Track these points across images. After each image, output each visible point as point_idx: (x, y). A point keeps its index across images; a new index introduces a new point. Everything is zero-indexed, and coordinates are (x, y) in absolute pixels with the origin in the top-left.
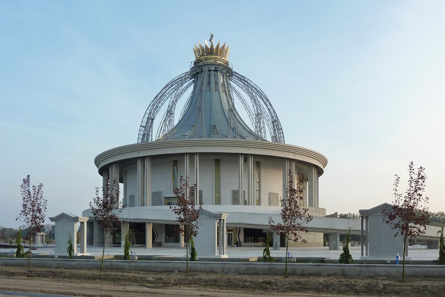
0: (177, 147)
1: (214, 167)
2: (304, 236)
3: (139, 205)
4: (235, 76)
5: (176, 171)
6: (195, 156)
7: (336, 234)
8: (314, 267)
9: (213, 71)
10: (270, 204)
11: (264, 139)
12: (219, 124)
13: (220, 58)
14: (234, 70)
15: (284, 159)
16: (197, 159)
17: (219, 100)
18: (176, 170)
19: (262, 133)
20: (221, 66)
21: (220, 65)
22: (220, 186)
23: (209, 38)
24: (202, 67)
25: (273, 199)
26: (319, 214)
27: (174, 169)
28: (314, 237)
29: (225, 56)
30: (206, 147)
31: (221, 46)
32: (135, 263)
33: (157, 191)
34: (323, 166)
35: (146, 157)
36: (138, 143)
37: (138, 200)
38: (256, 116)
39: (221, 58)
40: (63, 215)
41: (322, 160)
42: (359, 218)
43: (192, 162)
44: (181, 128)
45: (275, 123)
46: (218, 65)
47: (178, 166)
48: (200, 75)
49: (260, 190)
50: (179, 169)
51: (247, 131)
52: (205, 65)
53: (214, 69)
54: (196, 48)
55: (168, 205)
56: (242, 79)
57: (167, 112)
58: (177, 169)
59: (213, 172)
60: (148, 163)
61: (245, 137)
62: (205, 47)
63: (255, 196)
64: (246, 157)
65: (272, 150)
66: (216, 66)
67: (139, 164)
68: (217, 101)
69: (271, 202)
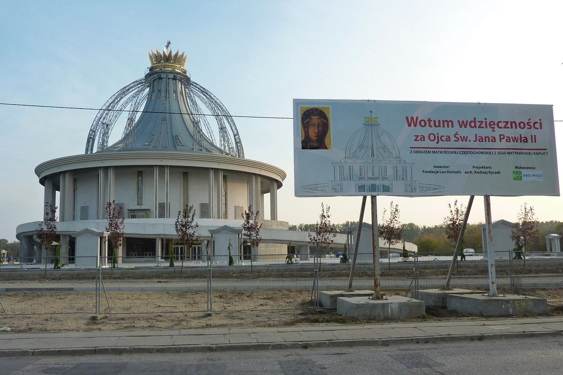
1: (182, 180)
2: (271, 249)
4: (193, 85)
5: (140, 182)
6: (165, 169)
7: (306, 246)
8: (331, 266)
9: (172, 79)
10: (236, 218)
11: (228, 152)
12: (181, 134)
13: (179, 66)
14: (192, 79)
15: (250, 174)
16: (167, 171)
17: (178, 109)
18: (141, 181)
20: (180, 75)
21: (179, 74)
22: (188, 199)
23: (166, 44)
24: (160, 74)
25: (239, 213)
26: (284, 227)
27: (138, 179)
28: (280, 250)
29: (183, 65)
31: (179, 54)
32: (196, 268)
33: (117, 203)
35: (66, 171)
38: (220, 129)
39: (180, 67)
40: (86, 230)
41: (280, 174)
42: (298, 231)
43: (162, 174)
44: (139, 136)
46: (177, 74)
47: (143, 176)
48: (158, 82)
49: (226, 204)
50: (144, 180)
51: (209, 142)
52: (163, 72)
53: (172, 77)
54: (152, 53)
55: (132, 218)
56: (204, 91)
58: (142, 180)
60: (111, 174)
61: (211, 151)
62: (162, 54)
63: (223, 209)
64: (216, 170)
65: (240, 166)
66: (175, 75)
67: (101, 173)
69: (236, 215)
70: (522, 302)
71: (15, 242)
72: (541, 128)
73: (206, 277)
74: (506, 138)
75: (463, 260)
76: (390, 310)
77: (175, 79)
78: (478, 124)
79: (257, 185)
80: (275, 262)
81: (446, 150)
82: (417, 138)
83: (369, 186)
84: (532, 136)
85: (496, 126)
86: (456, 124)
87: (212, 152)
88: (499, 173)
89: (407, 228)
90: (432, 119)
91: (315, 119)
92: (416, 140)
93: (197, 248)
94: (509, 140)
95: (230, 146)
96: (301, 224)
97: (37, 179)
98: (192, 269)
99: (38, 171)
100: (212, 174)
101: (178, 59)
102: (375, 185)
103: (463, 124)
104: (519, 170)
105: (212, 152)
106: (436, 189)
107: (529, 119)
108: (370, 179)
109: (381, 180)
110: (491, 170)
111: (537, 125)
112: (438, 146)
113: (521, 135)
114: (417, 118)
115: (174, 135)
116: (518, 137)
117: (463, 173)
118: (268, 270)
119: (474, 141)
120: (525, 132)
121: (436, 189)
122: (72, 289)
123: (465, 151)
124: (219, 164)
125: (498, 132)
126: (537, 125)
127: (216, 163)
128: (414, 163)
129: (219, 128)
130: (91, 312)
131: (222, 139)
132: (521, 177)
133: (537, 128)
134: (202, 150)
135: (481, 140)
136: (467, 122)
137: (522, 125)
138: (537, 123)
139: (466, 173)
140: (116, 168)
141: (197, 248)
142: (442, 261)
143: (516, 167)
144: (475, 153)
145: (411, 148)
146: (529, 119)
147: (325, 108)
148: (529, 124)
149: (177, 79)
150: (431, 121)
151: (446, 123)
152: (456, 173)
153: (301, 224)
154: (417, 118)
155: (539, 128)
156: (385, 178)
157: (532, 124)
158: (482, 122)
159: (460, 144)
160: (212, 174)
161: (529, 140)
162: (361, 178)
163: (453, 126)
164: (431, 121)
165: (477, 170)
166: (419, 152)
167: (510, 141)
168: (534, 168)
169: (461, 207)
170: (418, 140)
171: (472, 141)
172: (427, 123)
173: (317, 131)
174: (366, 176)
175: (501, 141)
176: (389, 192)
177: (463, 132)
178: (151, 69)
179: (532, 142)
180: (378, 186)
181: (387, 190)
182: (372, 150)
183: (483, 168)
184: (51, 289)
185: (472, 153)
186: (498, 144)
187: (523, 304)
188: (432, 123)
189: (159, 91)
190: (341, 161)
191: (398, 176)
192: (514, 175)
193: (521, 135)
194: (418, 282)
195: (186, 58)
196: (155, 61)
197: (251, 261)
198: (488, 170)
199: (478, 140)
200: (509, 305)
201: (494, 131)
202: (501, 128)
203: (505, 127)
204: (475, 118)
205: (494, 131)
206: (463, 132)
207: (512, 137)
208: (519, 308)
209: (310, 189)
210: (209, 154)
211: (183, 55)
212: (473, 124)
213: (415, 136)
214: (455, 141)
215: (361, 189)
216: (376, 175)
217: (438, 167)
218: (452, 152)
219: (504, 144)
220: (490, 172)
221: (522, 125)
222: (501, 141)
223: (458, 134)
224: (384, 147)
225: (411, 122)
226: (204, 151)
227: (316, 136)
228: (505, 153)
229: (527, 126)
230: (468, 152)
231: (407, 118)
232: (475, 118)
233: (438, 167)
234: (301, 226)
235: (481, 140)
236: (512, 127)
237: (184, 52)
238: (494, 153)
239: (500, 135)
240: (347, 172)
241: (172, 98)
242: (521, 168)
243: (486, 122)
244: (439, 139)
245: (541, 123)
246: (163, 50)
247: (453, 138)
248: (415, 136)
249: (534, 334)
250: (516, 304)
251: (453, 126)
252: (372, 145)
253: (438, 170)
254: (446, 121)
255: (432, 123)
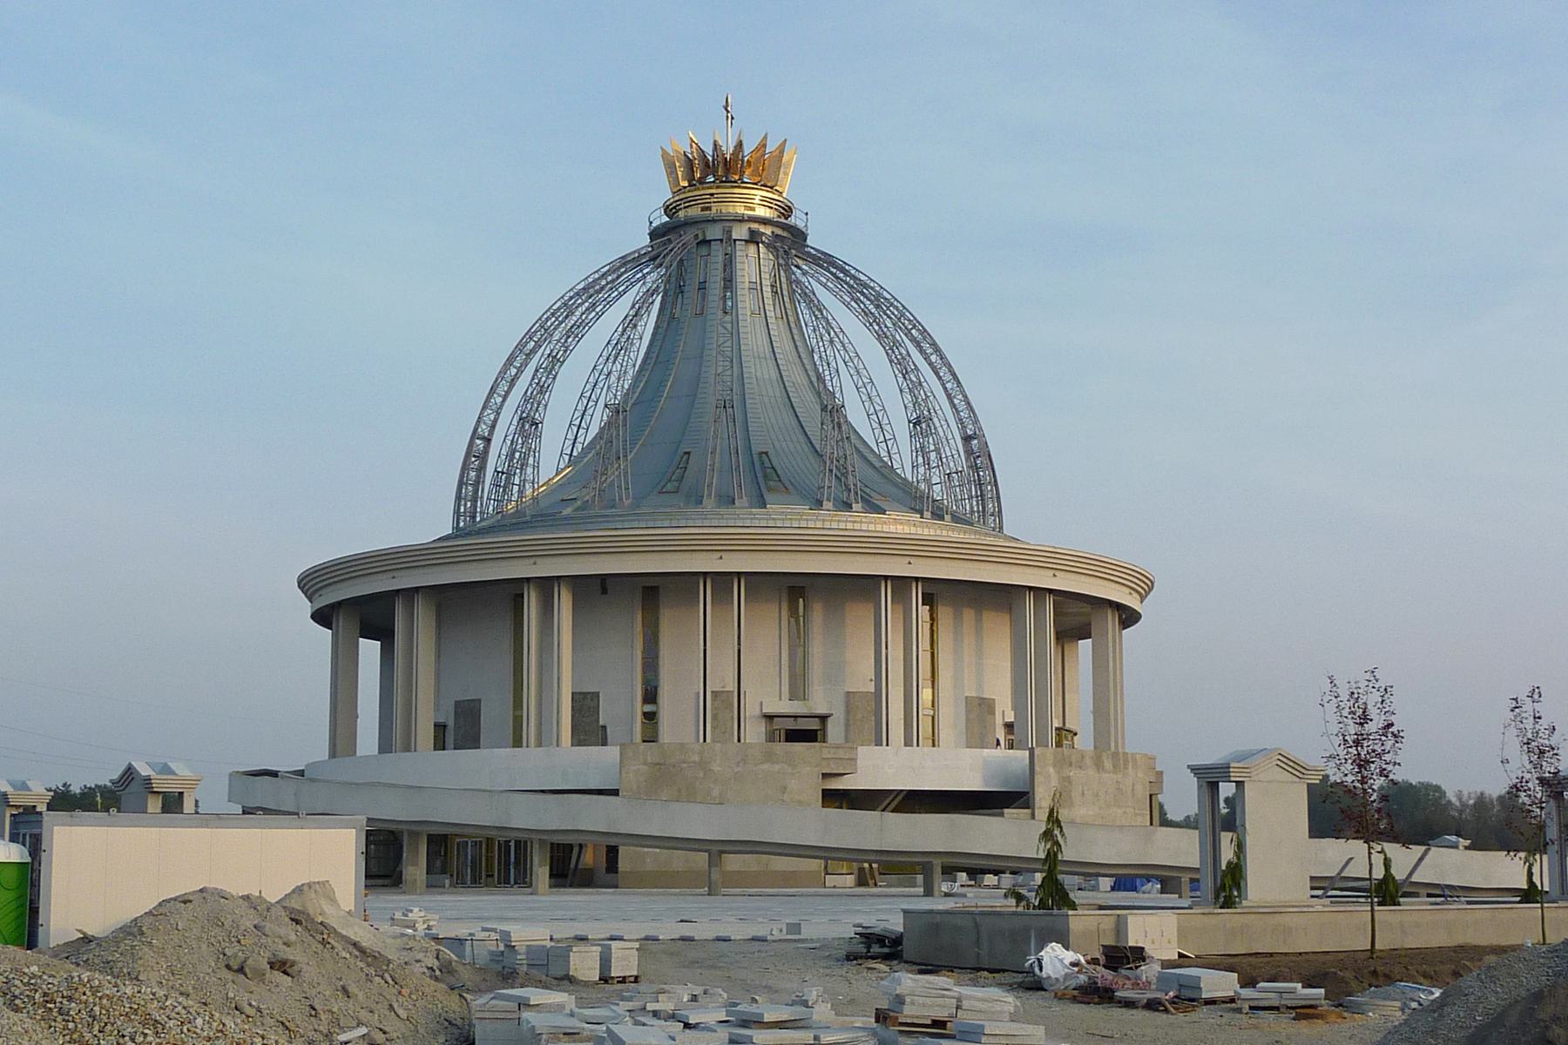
0: (370, 574)
3: (398, 749)
19: (917, 465)
30: (561, 559)
34: (1141, 597)
35: (417, 589)
36: (468, 529)
37: (494, 714)
38: (911, 425)
45: (921, 428)
56: (856, 287)
57: (515, 422)
59: (780, 613)
60: (564, 603)
66: (755, 226)
68: (768, 356)
71: (105, 785)
79: (1040, 622)
89: (1434, 795)
95: (952, 464)
97: (306, 608)
99: (310, 583)
100: (886, 593)
115: (756, 449)
124: (910, 563)
129: (910, 422)
131: (920, 460)
140: (578, 583)
149: (763, 242)
160: (886, 593)
178: (669, 210)
189: (699, 289)
241: (751, 373)
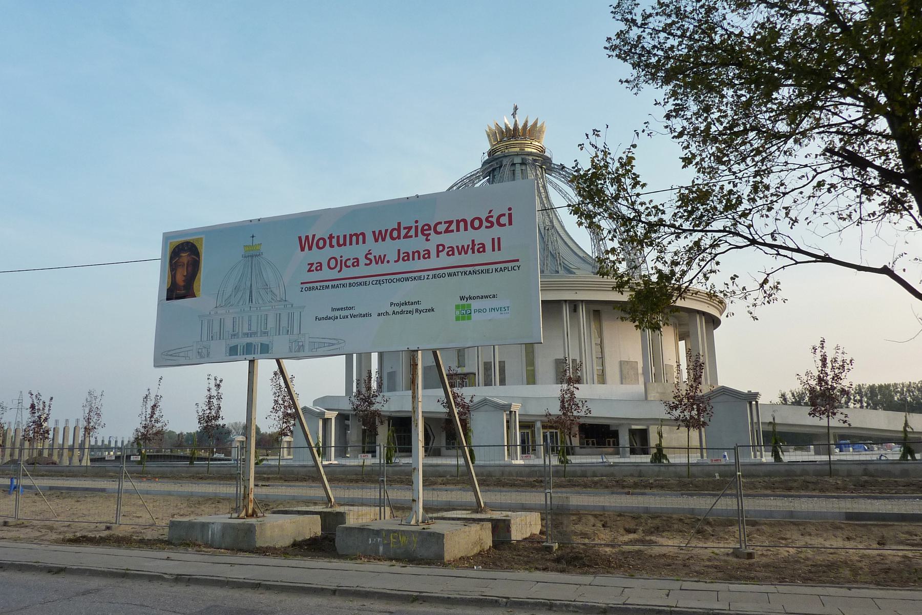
2: (682, 435)
10: (624, 381)
21: (530, 154)
23: (512, 111)
24: (500, 160)
31: (530, 124)
54: (490, 130)
66: (523, 157)
70: (401, 535)
72: (510, 223)
73: (377, 482)
74: (446, 250)
75: (909, 458)
76: (210, 533)
77: (523, 163)
78: (403, 232)
80: (679, 460)
81: (352, 281)
82: (311, 267)
83: (244, 346)
84: (493, 239)
85: (432, 232)
86: (370, 238)
87: (574, 273)
88: (433, 310)
90: (335, 235)
91: (185, 257)
92: (310, 271)
93: (548, 434)
94: (451, 252)
96: (859, 385)
98: (533, 469)
101: (531, 132)
102: (251, 344)
103: (379, 236)
104: (466, 303)
105: (574, 273)
106: (333, 344)
107: (490, 211)
108: (247, 335)
109: (259, 335)
110: (420, 307)
111: (504, 220)
112: (341, 276)
113: (473, 241)
114: (314, 236)
116: (468, 246)
117: (375, 315)
118: (503, 473)
119: (395, 262)
120: (484, 236)
121: (333, 344)
122: (103, 490)
123: (380, 279)
125: (435, 239)
126: (504, 220)
127: (570, 292)
128: (305, 307)
130: (759, 544)
132: (471, 313)
133: (505, 225)
134: (558, 272)
135: (407, 257)
136: (386, 231)
137: (475, 224)
138: (504, 215)
139: (379, 315)
141: (548, 434)
142: (860, 460)
143: (462, 298)
144: (395, 280)
145: (302, 283)
146: (490, 211)
147: (198, 240)
148: (490, 219)
150: (334, 237)
151: (354, 238)
152: (364, 316)
153: (859, 385)
154: (314, 236)
155: (507, 224)
156: (266, 333)
157: (494, 220)
158: (410, 228)
159: (375, 269)
161: (489, 247)
162: (235, 335)
163: (364, 242)
164: (334, 237)
165: (397, 309)
166: (313, 288)
167: (453, 254)
168: (494, 296)
169: (208, 379)
170: (313, 271)
171: (392, 262)
172: (328, 241)
173: (185, 274)
174: (240, 331)
175: (438, 256)
176: (268, 353)
177: (379, 249)
179: (494, 250)
180: (255, 346)
181: (265, 350)
182: (251, 292)
183: (406, 304)
184: (87, 489)
185: (390, 281)
186: (433, 262)
187: (403, 539)
188: (334, 242)
190: (210, 313)
191: (281, 328)
192: (458, 313)
193: (473, 241)
194: (237, 491)
195: (542, 127)
196: (494, 142)
197: (830, 461)
198: (415, 307)
199: (401, 259)
200: (379, 539)
201: (429, 240)
202: (441, 233)
203: (447, 231)
204: (399, 224)
205: (429, 240)
206: (379, 249)
207: (457, 247)
208: (395, 546)
209: (171, 355)
210: (571, 278)
211: (535, 124)
212: (395, 234)
213: (309, 264)
214: (366, 265)
215: (233, 353)
216: (254, 329)
217: (338, 310)
218: (482, 271)
219: (444, 260)
220: (417, 310)
221: (477, 224)
222: (438, 256)
223: (371, 254)
224: (266, 286)
225: (306, 243)
226: (562, 272)
227: (184, 281)
228: (444, 275)
229: (485, 224)
230: (385, 281)
231: (300, 238)
232: (399, 224)
233: (338, 310)
234: (860, 389)
235: (407, 257)
236: (458, 230)
237: (537, 119)
238: (426, 277)
239: (438, 246)
240: (216, 328)
242: (470, 298)
243: (417, 227)
244: (342, 264)
245: (510, 215)
246: (507, 121)
247: (363, 261)
248: (309, 264)
249: (128, 573)
250: (391, 537)
251: (364, 242)
252: (251, 285)
253: (337, 313)
254: (356, 234)
255: (334, 242)
